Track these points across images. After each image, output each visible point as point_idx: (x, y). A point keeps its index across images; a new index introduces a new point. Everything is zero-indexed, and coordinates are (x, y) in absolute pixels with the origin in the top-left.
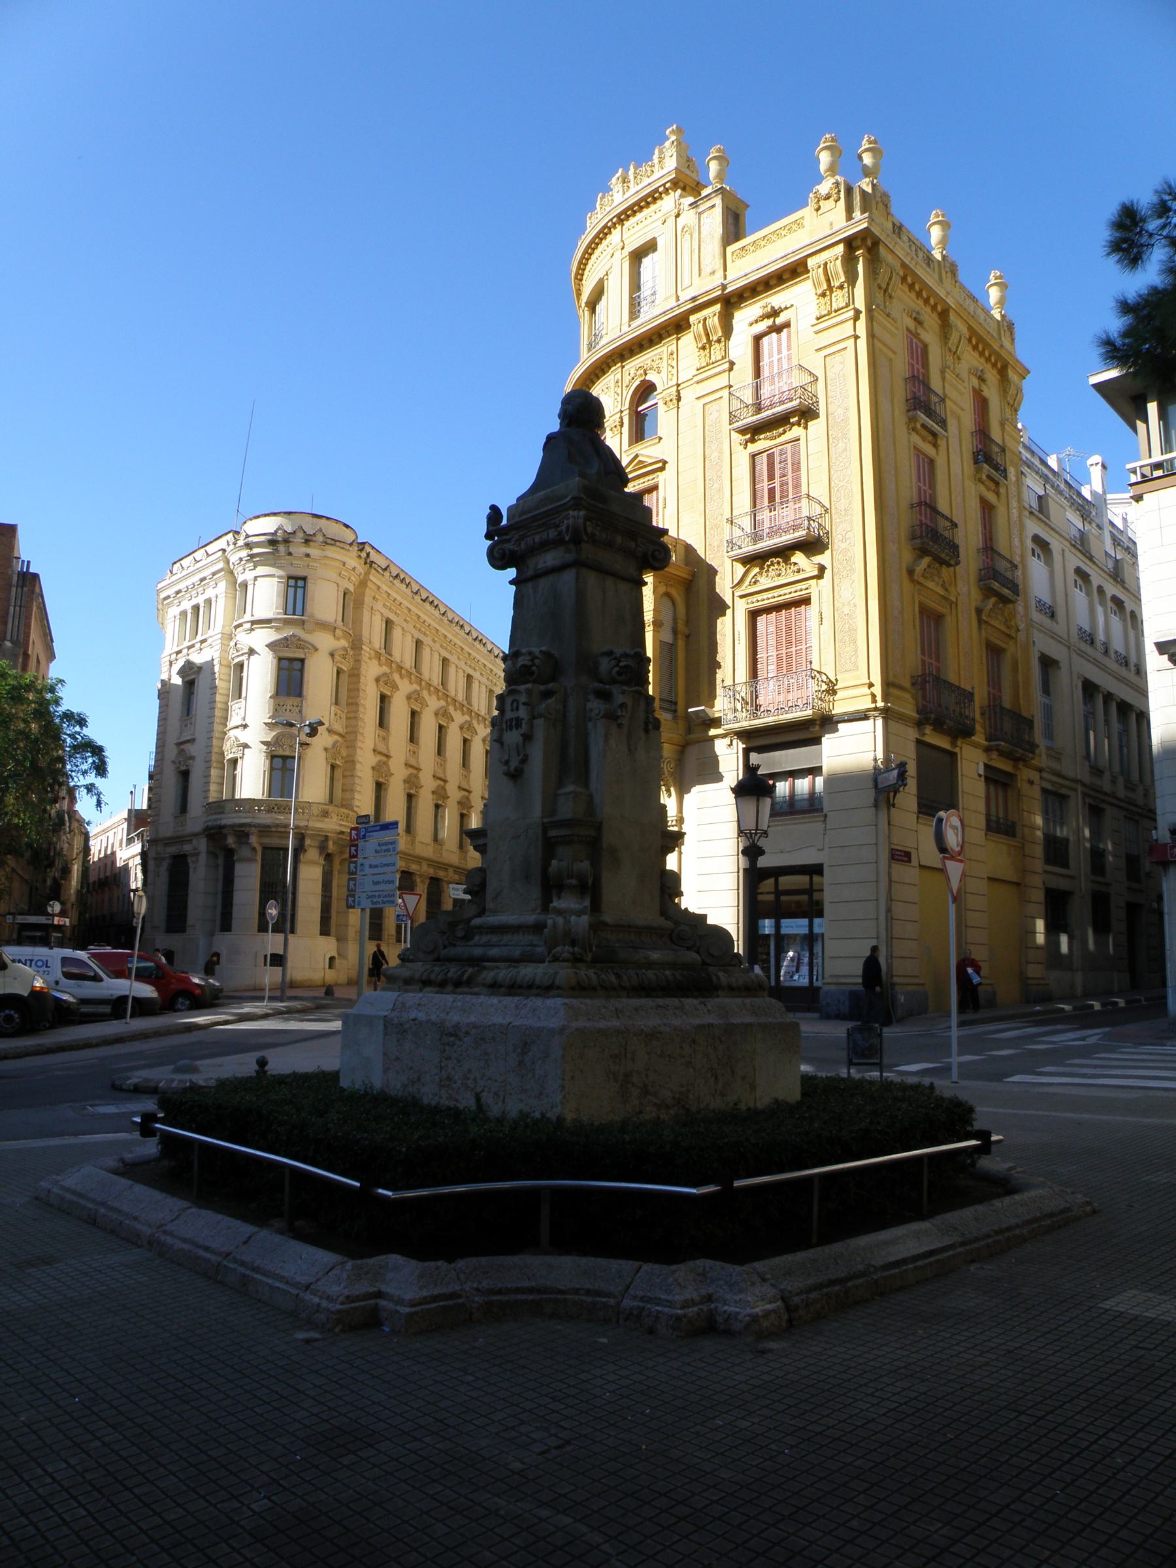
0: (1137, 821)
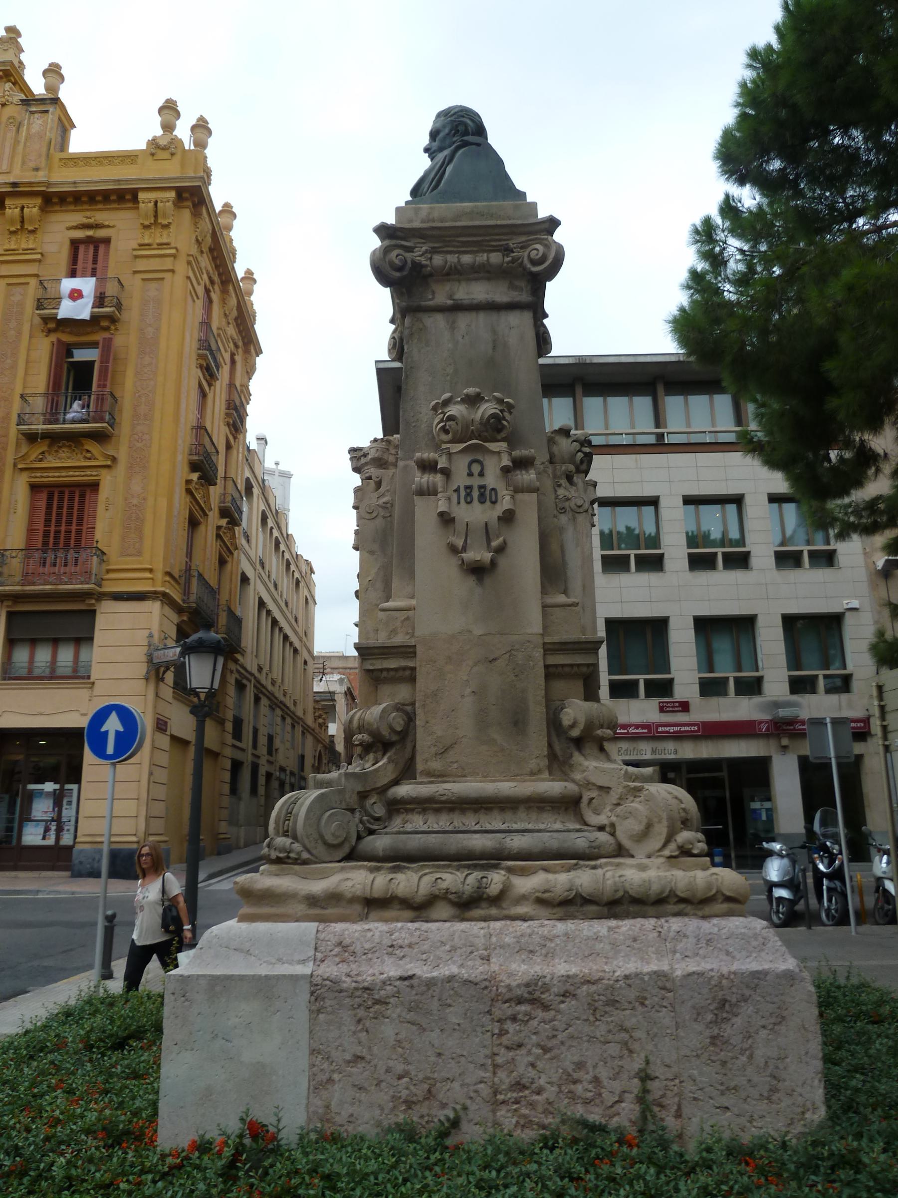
0: (274, 709)
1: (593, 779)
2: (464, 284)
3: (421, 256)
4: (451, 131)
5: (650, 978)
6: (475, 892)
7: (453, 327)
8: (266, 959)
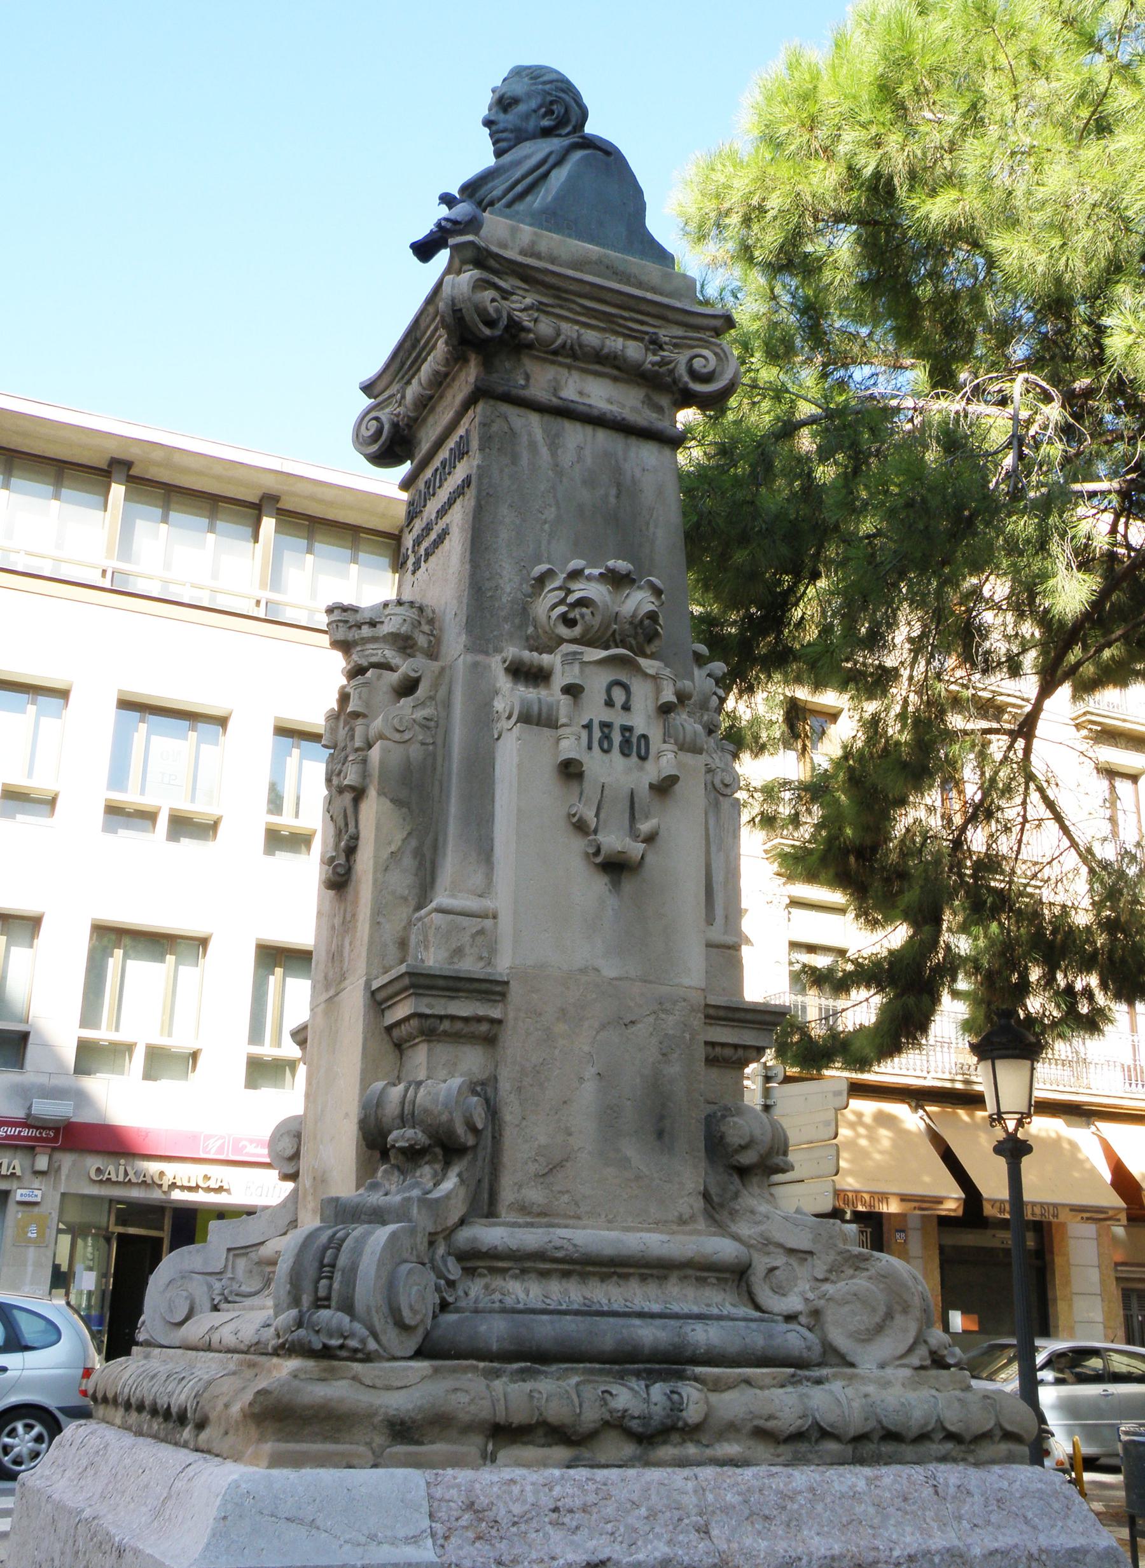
1: (778, 1236)
2: (576, 375)
3: (522, 310)
4: (540, 107)
5: (942, 1560)
6: (668, 1416)
7: (554, 445)
8: (348, 1536)
